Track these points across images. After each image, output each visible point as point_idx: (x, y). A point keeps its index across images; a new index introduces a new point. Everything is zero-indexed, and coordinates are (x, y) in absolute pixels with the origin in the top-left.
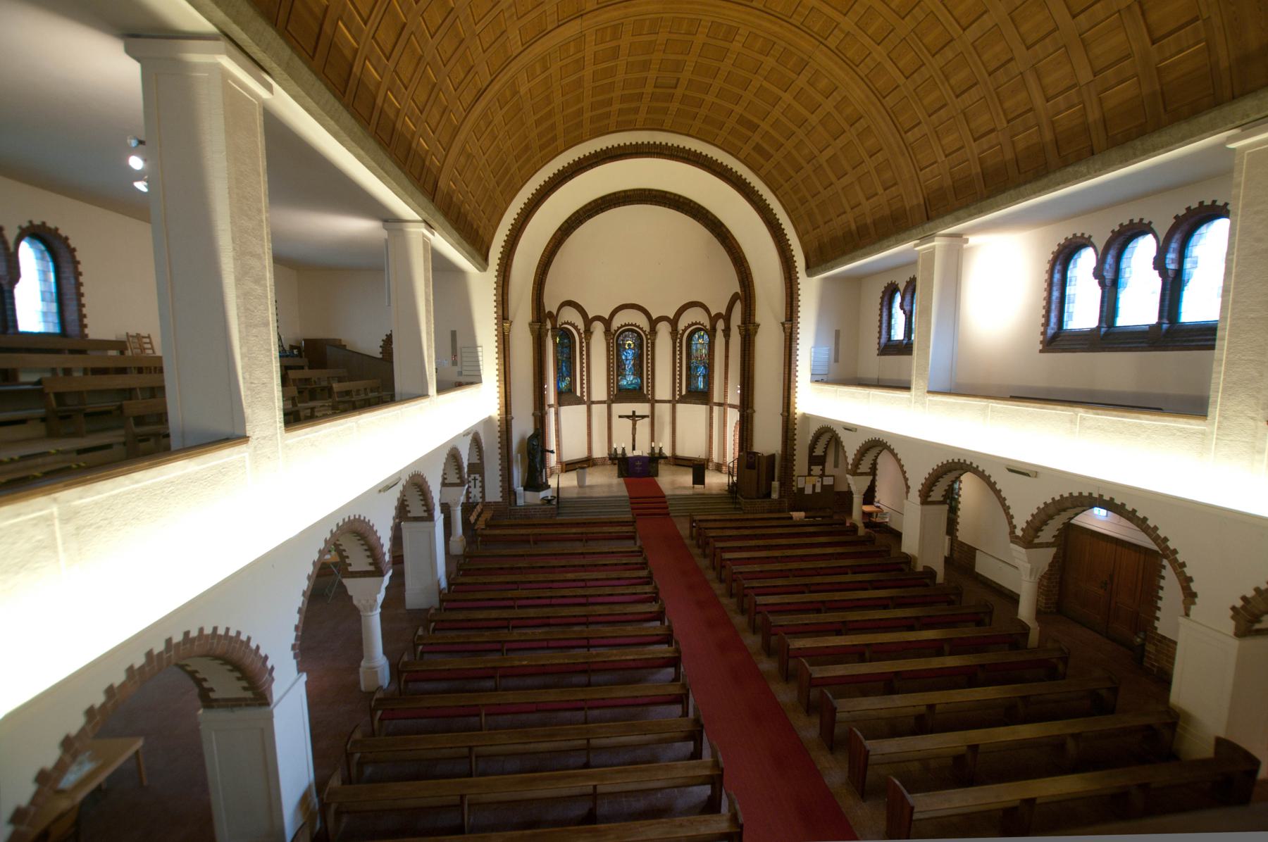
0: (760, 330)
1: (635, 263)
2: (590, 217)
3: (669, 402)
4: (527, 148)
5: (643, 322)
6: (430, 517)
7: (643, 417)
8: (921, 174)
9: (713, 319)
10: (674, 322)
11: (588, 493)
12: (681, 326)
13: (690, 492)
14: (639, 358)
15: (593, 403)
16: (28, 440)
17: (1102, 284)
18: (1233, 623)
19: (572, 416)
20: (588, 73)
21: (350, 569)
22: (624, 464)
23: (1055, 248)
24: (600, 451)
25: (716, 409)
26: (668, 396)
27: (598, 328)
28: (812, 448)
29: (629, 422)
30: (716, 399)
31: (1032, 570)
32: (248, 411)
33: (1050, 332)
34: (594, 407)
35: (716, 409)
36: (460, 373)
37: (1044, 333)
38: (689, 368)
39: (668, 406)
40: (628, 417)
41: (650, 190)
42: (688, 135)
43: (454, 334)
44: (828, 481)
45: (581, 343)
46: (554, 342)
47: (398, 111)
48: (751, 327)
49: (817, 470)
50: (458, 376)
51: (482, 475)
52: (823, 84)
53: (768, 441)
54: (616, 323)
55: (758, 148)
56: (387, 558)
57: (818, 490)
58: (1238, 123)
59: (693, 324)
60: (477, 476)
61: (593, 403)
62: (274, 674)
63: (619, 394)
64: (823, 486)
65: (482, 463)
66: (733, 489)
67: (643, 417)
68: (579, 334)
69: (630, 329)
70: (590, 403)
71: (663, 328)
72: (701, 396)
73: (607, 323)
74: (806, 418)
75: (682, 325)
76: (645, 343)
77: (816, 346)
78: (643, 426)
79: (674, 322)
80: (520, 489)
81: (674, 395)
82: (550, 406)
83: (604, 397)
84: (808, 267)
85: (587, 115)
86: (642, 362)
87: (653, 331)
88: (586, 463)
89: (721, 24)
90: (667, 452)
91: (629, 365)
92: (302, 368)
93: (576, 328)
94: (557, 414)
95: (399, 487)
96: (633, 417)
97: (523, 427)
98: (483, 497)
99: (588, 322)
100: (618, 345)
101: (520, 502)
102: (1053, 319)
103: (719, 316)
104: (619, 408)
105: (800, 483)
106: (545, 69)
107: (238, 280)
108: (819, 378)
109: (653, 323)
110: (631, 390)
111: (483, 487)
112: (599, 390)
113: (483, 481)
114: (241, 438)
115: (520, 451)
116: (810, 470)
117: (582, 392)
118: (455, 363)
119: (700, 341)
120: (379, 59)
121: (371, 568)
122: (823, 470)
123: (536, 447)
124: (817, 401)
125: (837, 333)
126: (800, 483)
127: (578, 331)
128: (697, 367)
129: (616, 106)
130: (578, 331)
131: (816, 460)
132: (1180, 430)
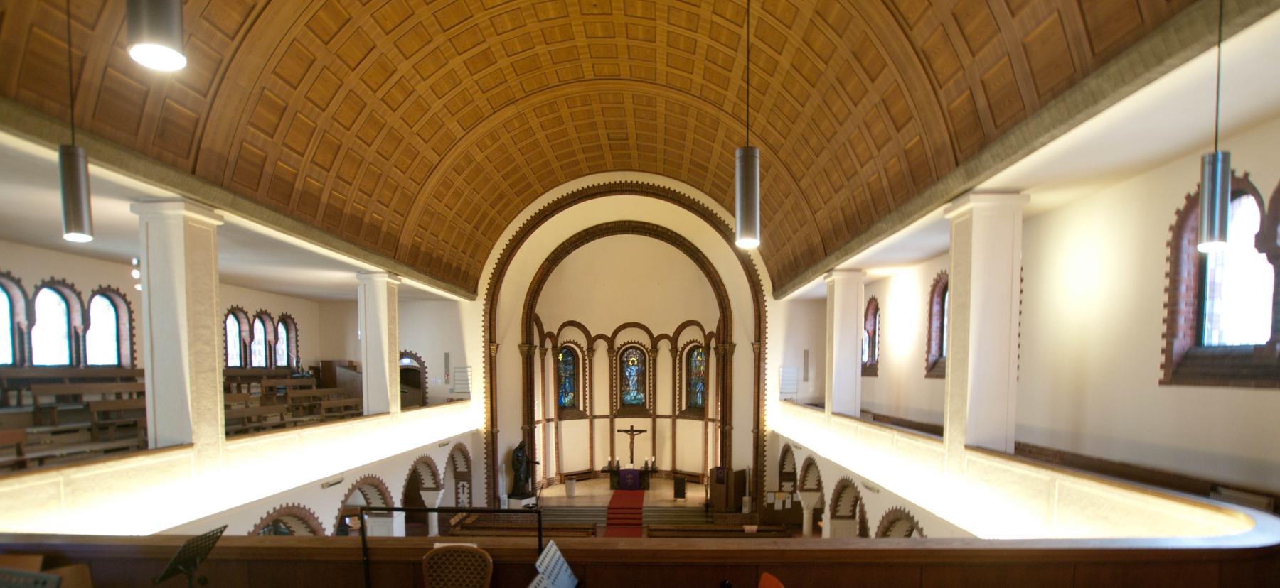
0: (736, 350)
1: (624, 284)
2: (576, 247)
5: (645, 340)
7: (641, 432)
9: (708, 337)
10: (674, 340)
11: (578, 503)
12: (680, 344)
13: (669, 505)
14: (642, 374)
15: (596, 417)
16: (79, 443)
19: (574, 430)
22: (614, 474)
23: (932, 282)
24: (599, 465)
25: (710, 424)
26: (668, 412)
27: (601, 346)
29: (627, 436)
32: (194, 427)
33: (932, 359)
34: (596, 421)
35: (710, 424)
36: (452, 391)
38: (689, 384)
39: (669, 421)
40: (626, 431)
46: (557, 361)
48: (727, 347)
49: (788, 486)
50: (458, 396)
51: (470, 482)
53: (742, 458)
54: (619, 341)
57: (788, 505)
58: (947, 198)
59: (691, 342)
61: (596, 417)
63: (623, 409)
65: (470, 471)
66: (708, 505)
67: (641, 432)
68: (583, 352)
69: (632, 346)
70: (593, 418)
71: (664, 346)
72: (695, 411)
73: (610, 341)
74: (775, 436)
75: (681, 342)
76: (648, 358)
77: (784, 366)
78: (643, 442)
79: (674, 340)
80: (503, 496)
81: (674, 411)
82: (539, 422)
83: (607, 412)
87: (655, 349)
88: (586, 476)
90: (665, 466)
91: (633, 380)
92: (310, 387)
93: (579, 346)
94: (557, 428)
95: (342, 490)
96: (632, 432)
97: (510, 438)
98: (470, 503)
99: (591, 341)
100: (622, 362)
102: (1184, 322)
105: (770, 498)
107: (191, 345)
108: (788, 397)
111: (470, 493)
112: (602, 404)
113: (470, 488)
114: (191, 445)
115: (506, 462)
116: (781, 486)
118: (447, 382)
119: (698, 358)
123: (523, 459)
124: (786, 421)
125: (806, 353)
126: (770, 498)
127: (581, 349)
130: (581, 349)
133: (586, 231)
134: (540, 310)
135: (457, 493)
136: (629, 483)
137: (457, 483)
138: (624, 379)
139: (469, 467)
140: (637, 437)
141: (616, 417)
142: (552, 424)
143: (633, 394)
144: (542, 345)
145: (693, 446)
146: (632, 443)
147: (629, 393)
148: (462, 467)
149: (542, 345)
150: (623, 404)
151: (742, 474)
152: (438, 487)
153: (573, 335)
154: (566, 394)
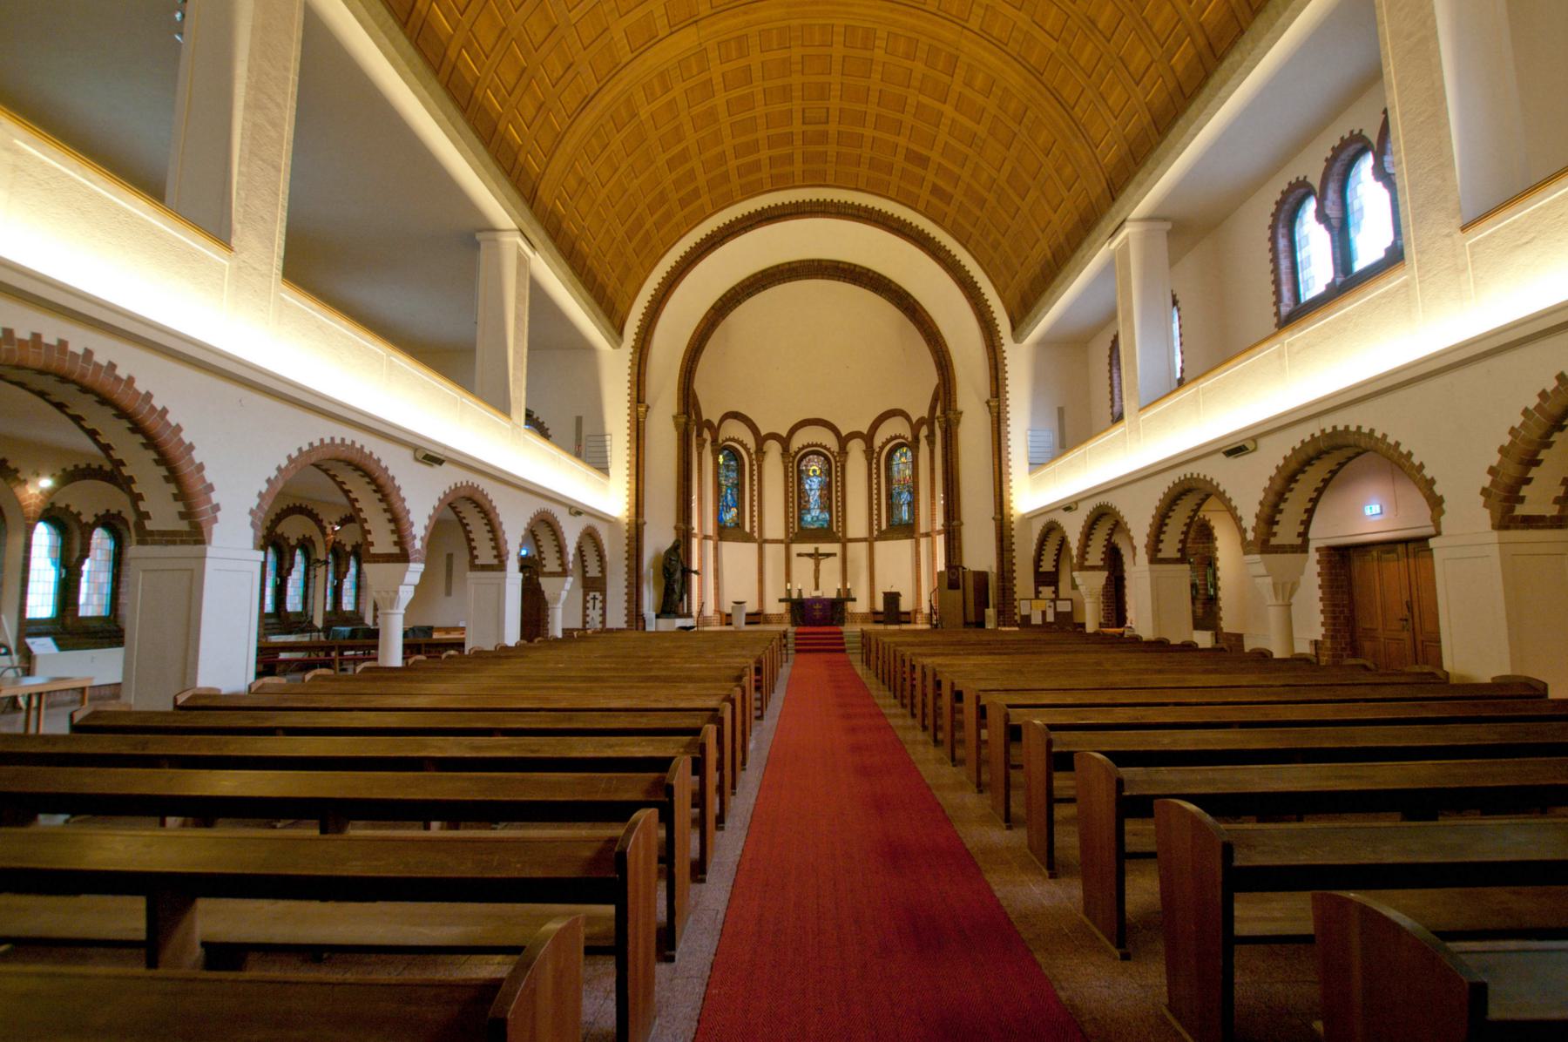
1: (814, 362)
2: (750, 295)
3: (864, 540)
4: (662, 198)
5: (830, 441)
6: (501, 566)
8: (1097, 151)
10: (868, 438)
12: (878, 442)
14: (827, 488)
15: (766, 541)
17: (1329, 228)
18: (1487, 512)
19: (738, 555)
20: (720, 100)
21: (373, 550)
22: (800, 609)
25: (923, 541)
26: (863, 533)
27: (773, 449)
28: (1038, 561)
29: (810, 562)
30: (923, 529)
31: (1275, 585)
34: (767, 547)
37: (1277, 314)
38: (890, 496)
39: (863, 546)
40: (810, 555)
41: (820, 261)
42: (857, 189)
43: (579, 420)
44: (1064, 607)
45: (751, 465)
47: (478, 79)
48: (951, 416)
49: (1047, 591)
51: (603, 592)
52: (979, 81)
53: (980, 555)
54: (797, 443)
55: (936, 190)
56: (418, 544)
57: (1050, 618)
59: (893, 438)
60: (598, 595)
61: (766, 541)
62: (219, 514)
63: (799, 533)
64: (1057, 614)
69: (814, 450)
70: (762, 542)
72: (907, 530)
73: (785, 442)
78: (831, 567)
83: (781, 535)
84: (1014, 328)
85: (733, 163)
86: (830, 492)
87: (843, 451)
89: (854, 28)
93: (744, 446)
94: (716, 548)
97: (658, 539)
98: (603, 622)
99: (761, 440)
101: (650, 628)
103: (921, 421)
104: (797, 548)
106: (666, 89)
109: (843, 441)
110: (815, 532)
111: (604, 609)
112: (775, 525)
113: (604, 601)
116: (1037, 593)
117: (752, 527)
119: (902, 461)
120: (478, 56)
121: (396, 550)
122: (1056, 592)
123: (675, 573)
126: (1023, 608)
128: (899, 494)
129: (764, 154)
131: (1046, 579)
132: (1383, 296)
133: (763, 272)
134: (699, 386)
135: (585, 608)
136: (817, 618)
137: (585, 595)
138: (802, 494)
139: (603, 570)
140: (824, 563)
141: (793, 541)
142: (710, 544)
143: (815, 513)
144: (699, 435)
145: (904, 571)
146: (817, 571)
147: (809, 511)
148: (593, 571)
149: (699, 435)
150: (801, 528)
151: (981, 578)
152: (564, 573)
153: (734, 430)
154: (728, 508)
